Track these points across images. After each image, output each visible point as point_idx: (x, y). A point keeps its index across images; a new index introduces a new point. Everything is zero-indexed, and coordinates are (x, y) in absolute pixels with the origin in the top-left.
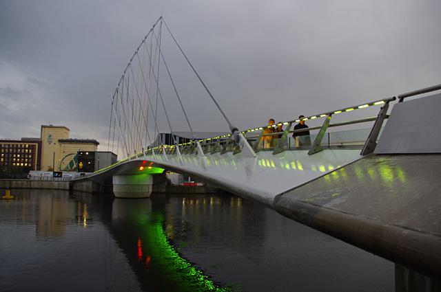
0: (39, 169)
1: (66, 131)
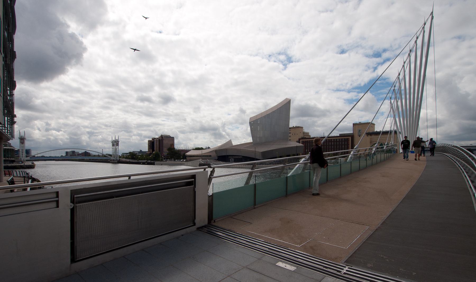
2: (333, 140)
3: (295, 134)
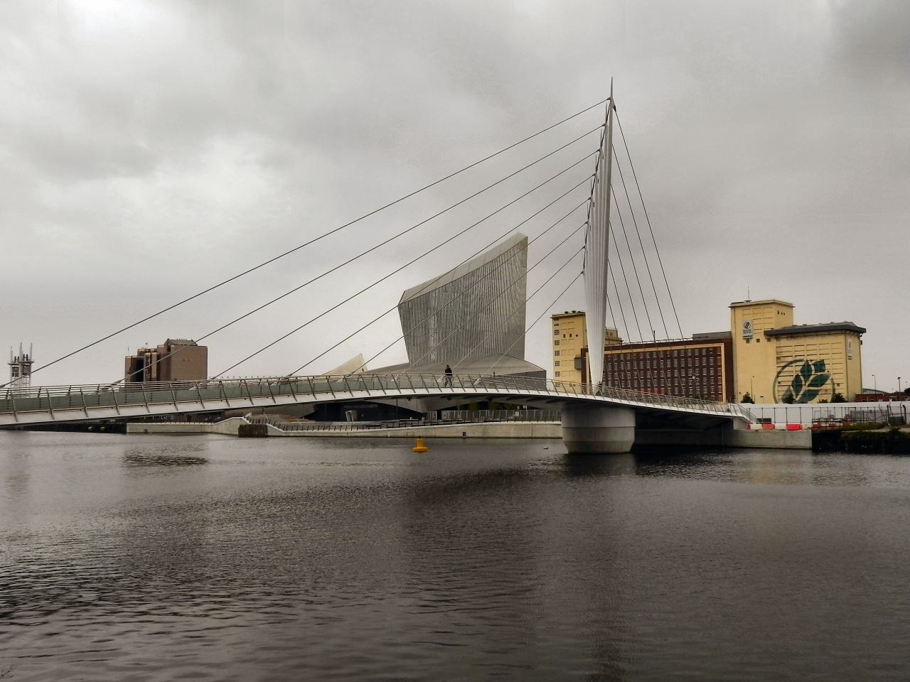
0: (731, 398)
1: (782, 309)
2: (662, 356)
3: (571, 335)
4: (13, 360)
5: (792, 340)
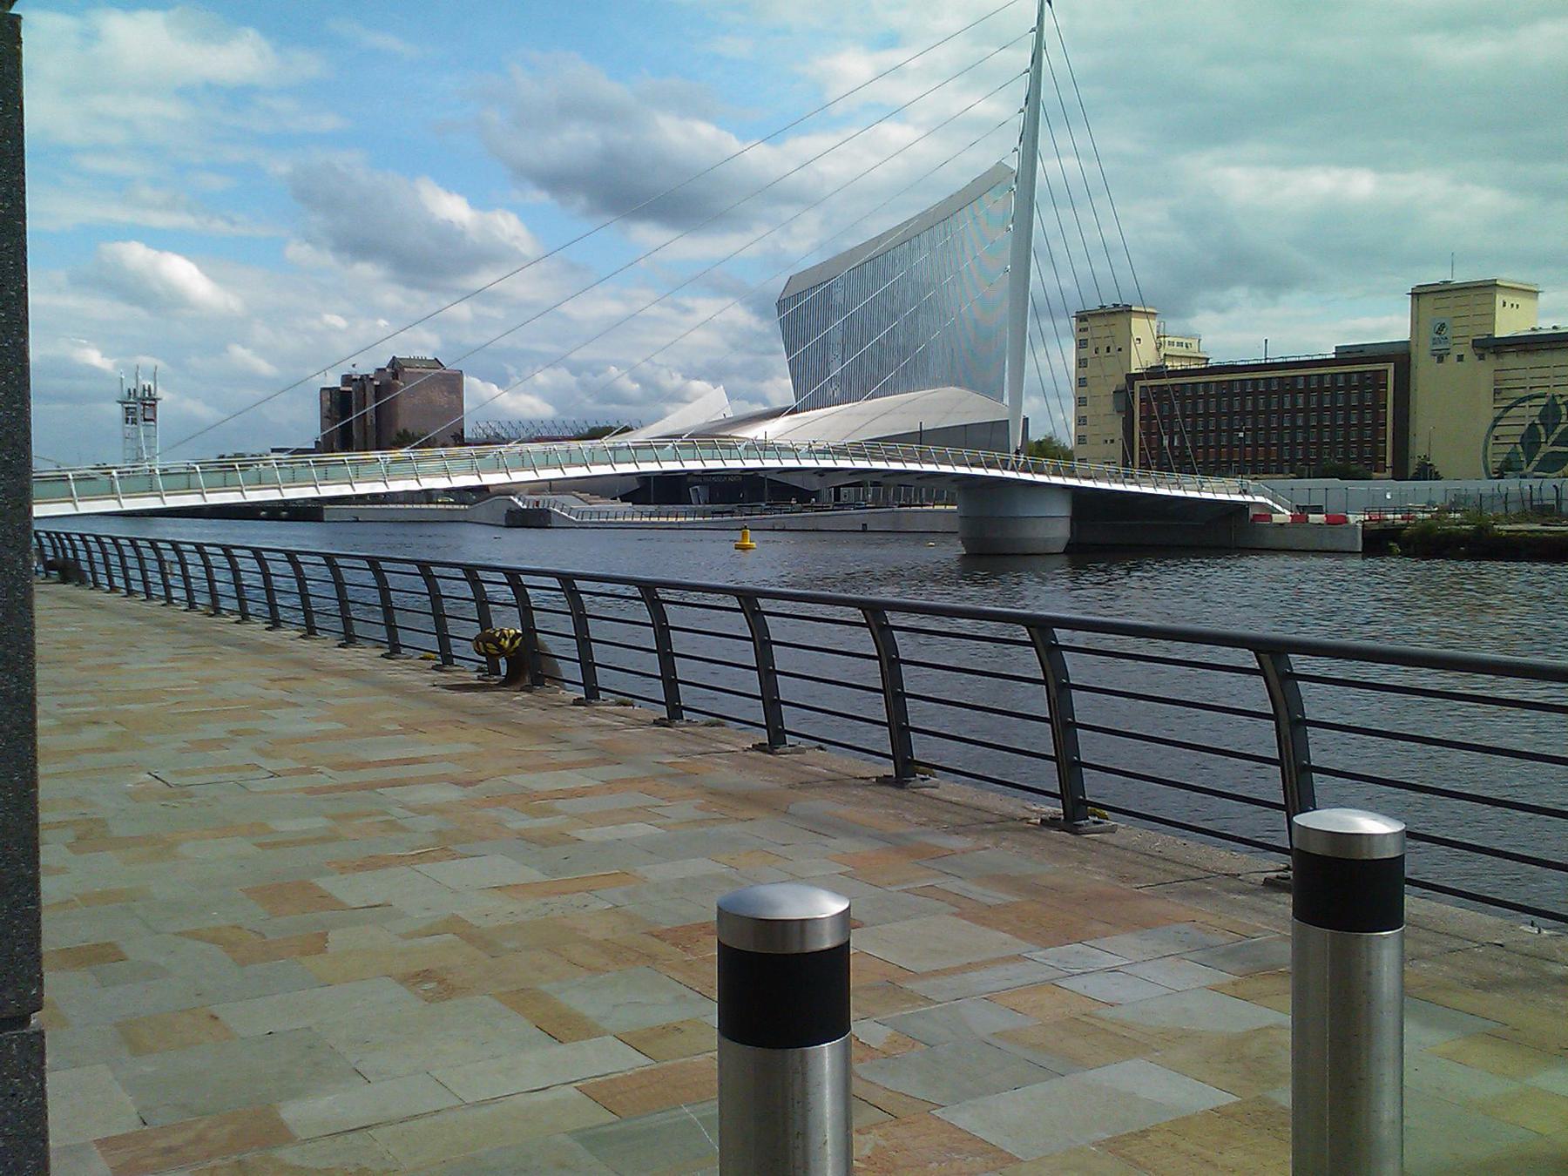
2: (1355, 380)
4: (126, 393)
5: (1528, 355)
